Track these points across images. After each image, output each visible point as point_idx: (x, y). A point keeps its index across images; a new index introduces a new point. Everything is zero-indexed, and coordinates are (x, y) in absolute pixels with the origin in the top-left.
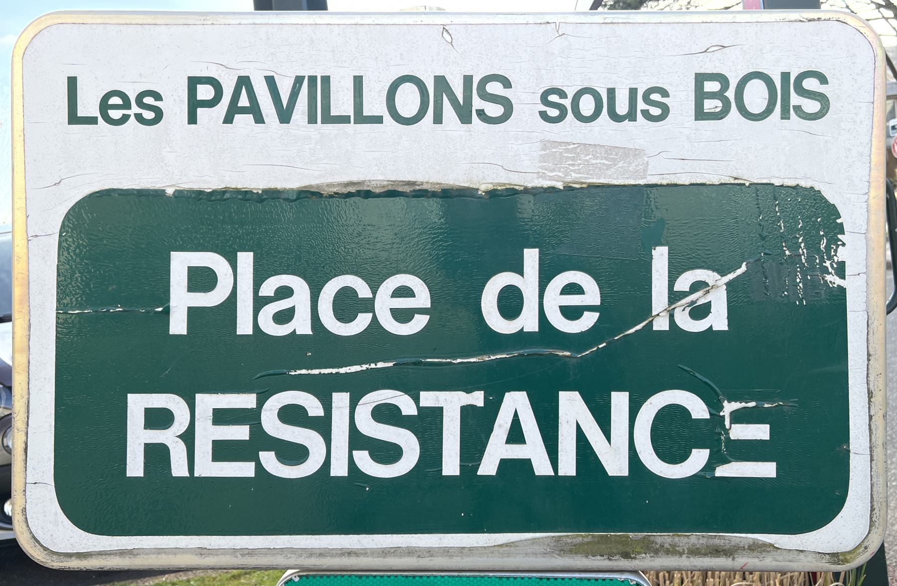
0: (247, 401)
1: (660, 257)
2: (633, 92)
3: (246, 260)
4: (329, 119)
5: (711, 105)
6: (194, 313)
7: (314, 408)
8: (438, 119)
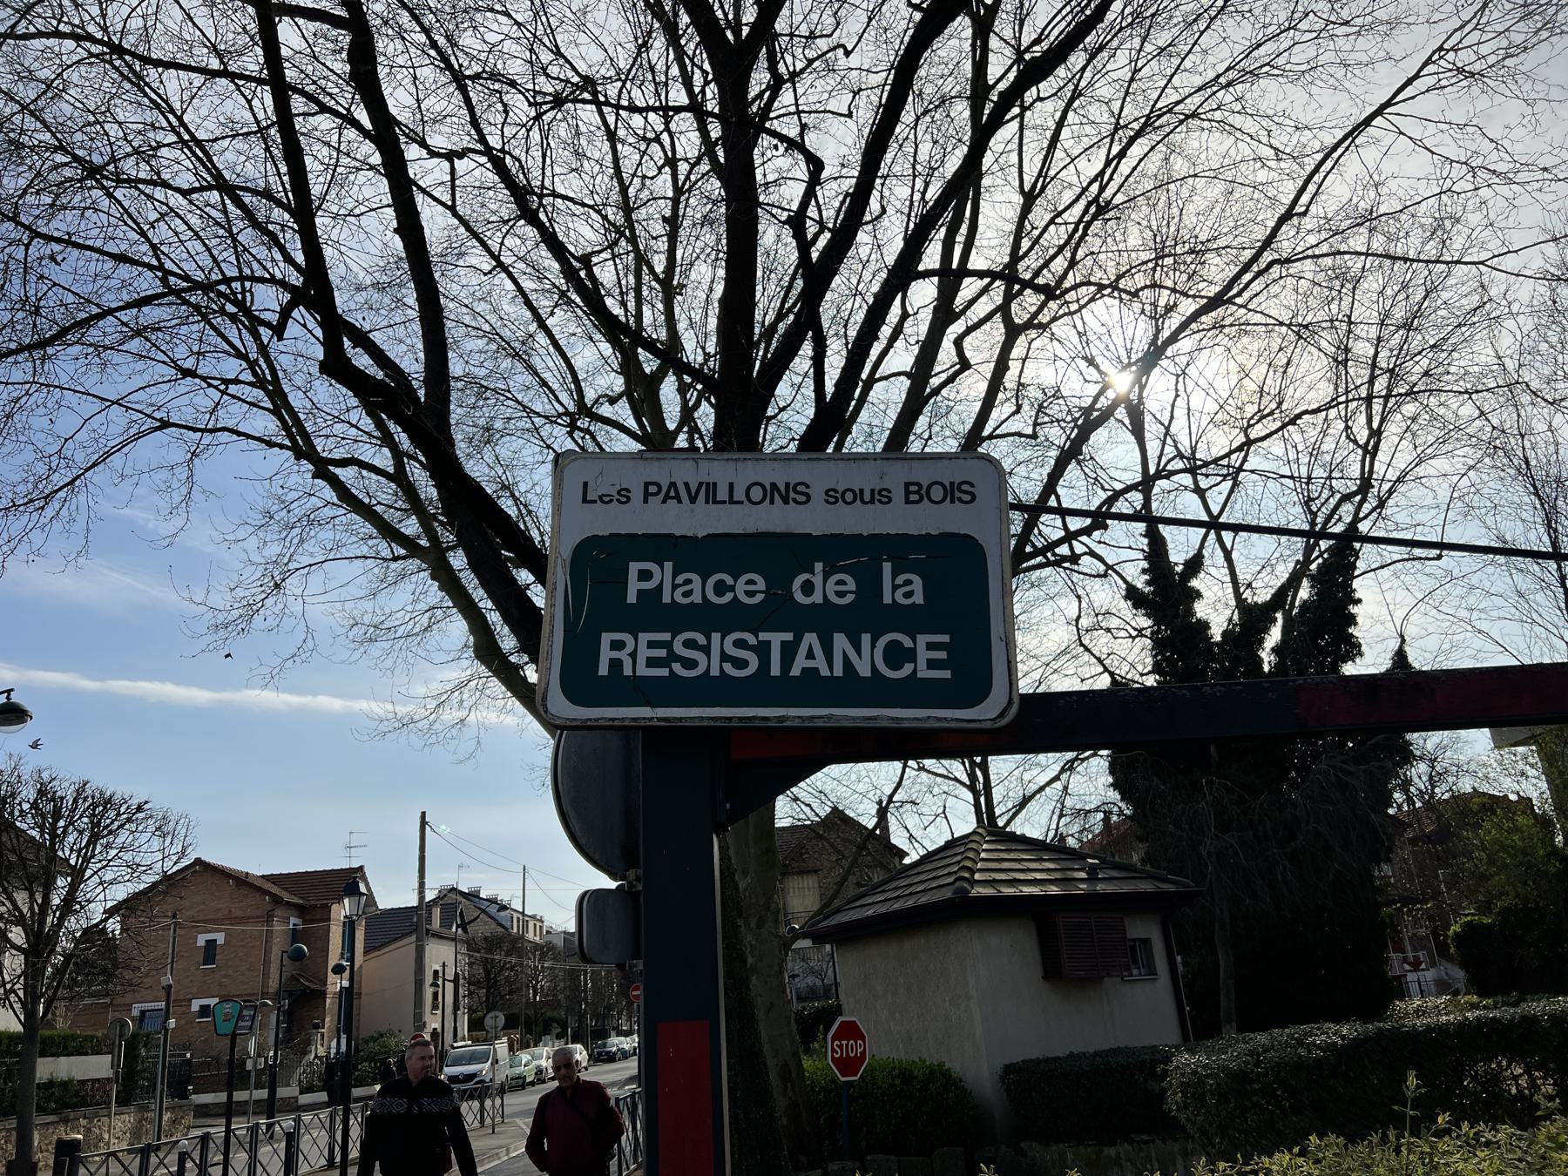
0: (666, 636)
1: (887, 567)
2: (873, 491)
3: (668, 566)
4: (715, 502)
5: (914, 497)
6: (639, 591)
7: (702, 640)
8: (772, 502)
